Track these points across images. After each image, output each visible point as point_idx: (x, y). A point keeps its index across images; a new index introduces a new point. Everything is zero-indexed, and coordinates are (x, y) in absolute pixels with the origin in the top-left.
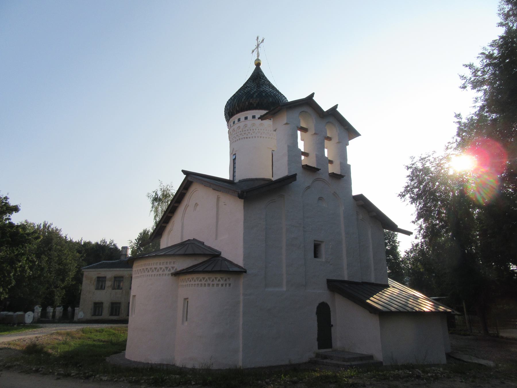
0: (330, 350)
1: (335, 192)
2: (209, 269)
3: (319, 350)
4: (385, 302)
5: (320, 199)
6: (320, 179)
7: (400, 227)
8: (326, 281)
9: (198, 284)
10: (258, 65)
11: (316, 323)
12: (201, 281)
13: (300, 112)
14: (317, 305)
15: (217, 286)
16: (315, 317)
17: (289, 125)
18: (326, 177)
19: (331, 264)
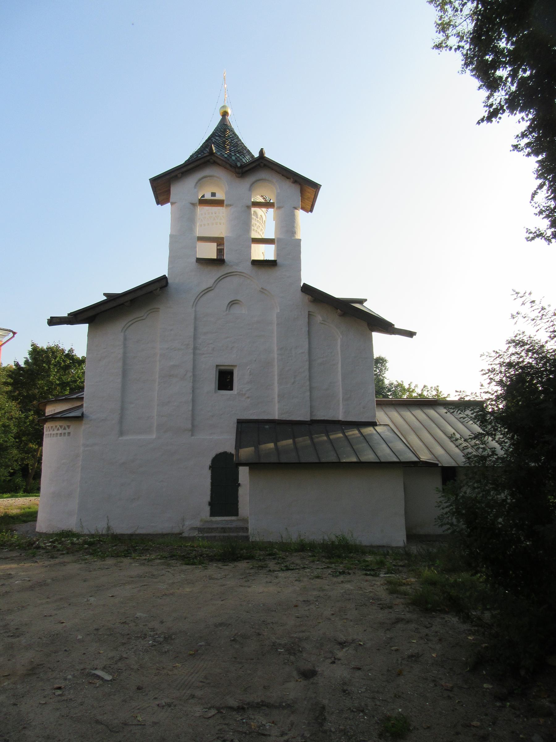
0: (233, 518)
1: (262, 288)
2: (456, 416)
3: (212, 518)
4: (371, 449)
5: (233, 303)
6: (232, 274)
7: (397, 326)
8: (236, 421)
9: (57, 434)
10: (225, 114)
11: (209, 481)
12: (65, 429)
13: (197, 183)
14: (213, 455)
15: (60, 436)
16: (208, 474)
17: (176, 204)
18: (247, 268)
19: (248, 397)
